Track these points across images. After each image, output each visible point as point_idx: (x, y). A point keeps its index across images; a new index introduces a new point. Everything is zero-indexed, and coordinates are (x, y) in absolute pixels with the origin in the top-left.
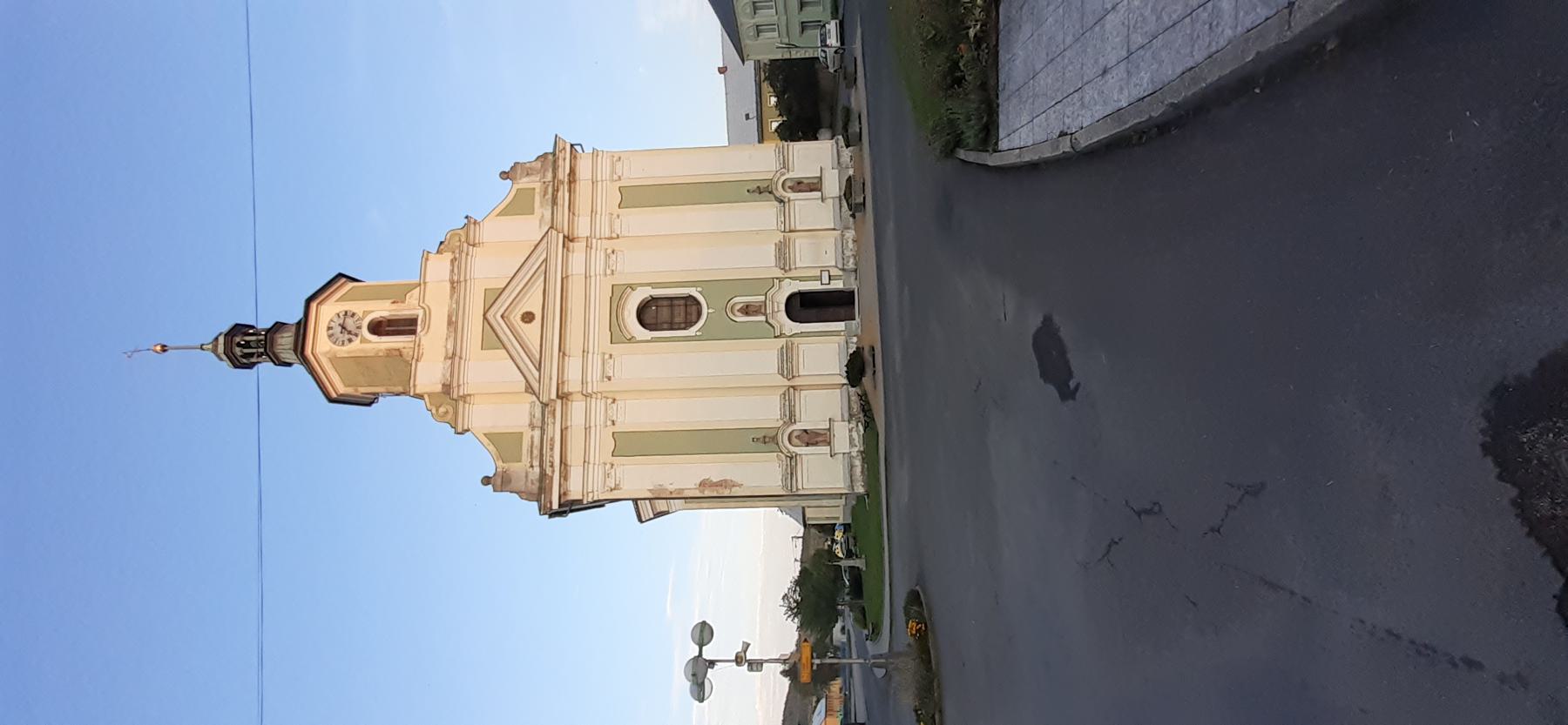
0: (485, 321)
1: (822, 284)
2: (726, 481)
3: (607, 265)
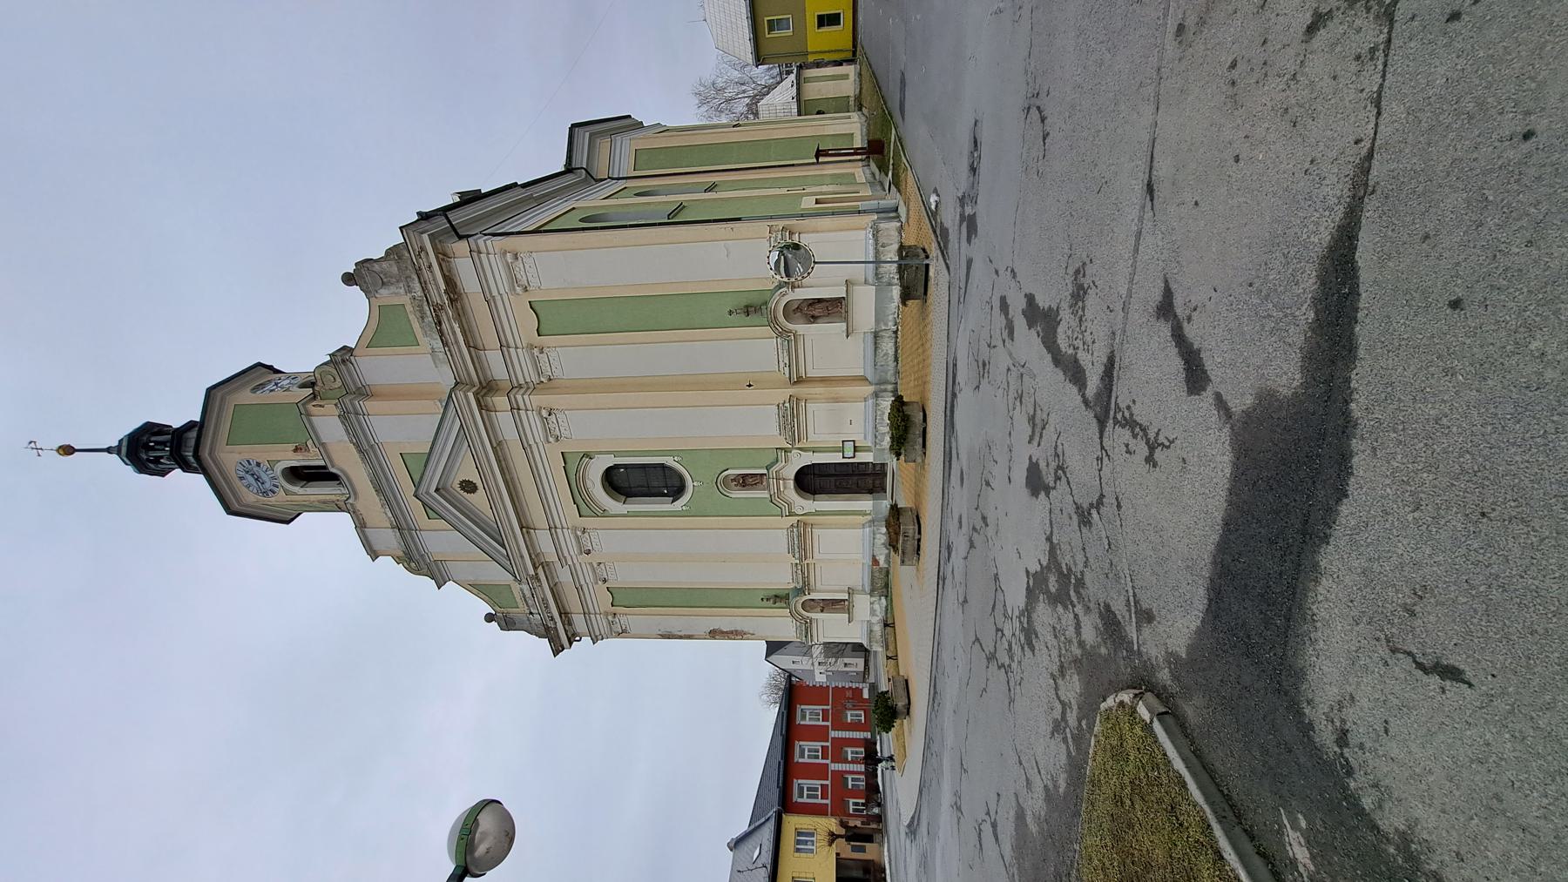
0: (417, 479)
1: (843, 457)
2: (736, 631)
3: (547, 431)
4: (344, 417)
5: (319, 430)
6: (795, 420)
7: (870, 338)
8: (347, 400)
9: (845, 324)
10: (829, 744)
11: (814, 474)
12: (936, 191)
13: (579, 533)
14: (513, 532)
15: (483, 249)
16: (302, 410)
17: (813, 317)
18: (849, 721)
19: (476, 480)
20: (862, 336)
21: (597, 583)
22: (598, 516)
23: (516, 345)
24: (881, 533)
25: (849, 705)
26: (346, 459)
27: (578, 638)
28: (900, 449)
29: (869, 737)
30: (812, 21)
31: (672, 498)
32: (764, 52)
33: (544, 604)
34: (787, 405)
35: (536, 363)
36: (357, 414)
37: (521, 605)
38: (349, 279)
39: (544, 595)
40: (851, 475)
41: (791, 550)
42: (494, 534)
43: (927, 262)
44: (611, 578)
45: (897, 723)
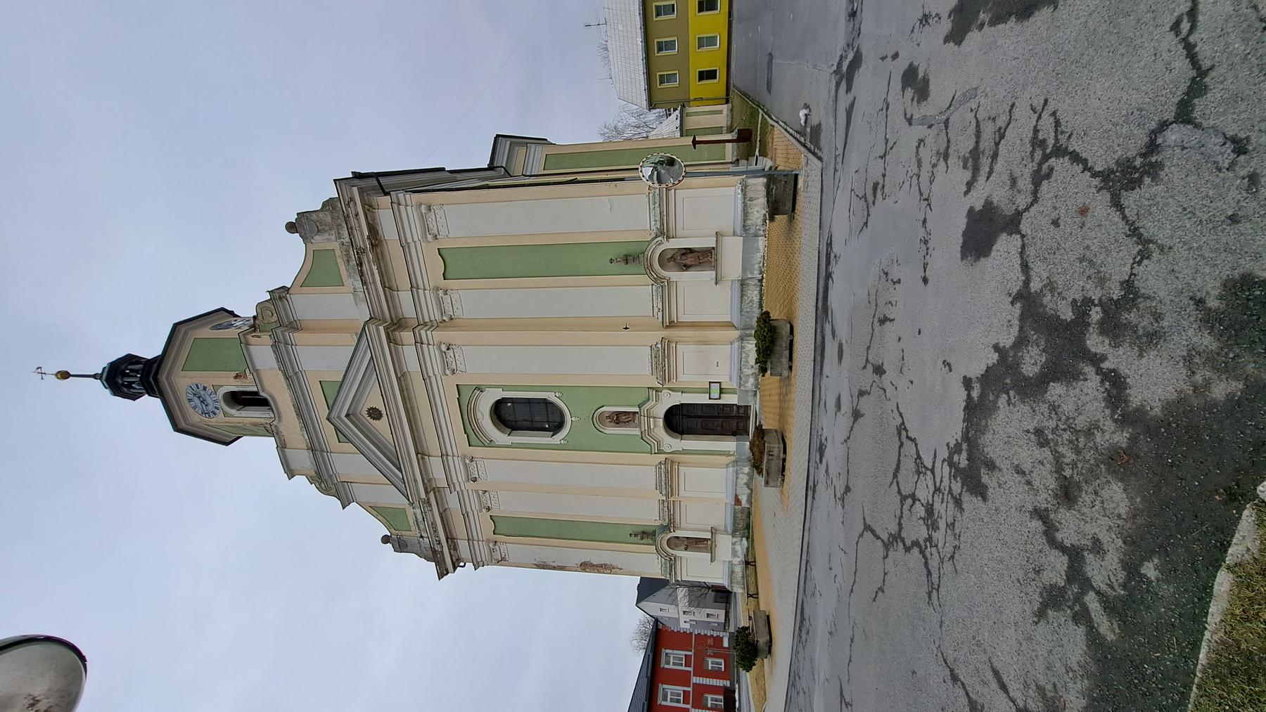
0: (330, 404)
1: (710, 399)
2: (605, 565)
3: (445, 365)
4: (275, 346)
5: (254, 357)
6: (666, 360)
7: (737, 286)
8: (279, 331)
9: (714, 273)
10: (690, 689)
11: (682, 415)
12: (807, 106)
13: (467, 461)
14: (410, 457)
15: (402, 201)
16: (243, 341)
17: (685, 266)
18: (710, 668)
19: (382, 408)
20: (730, 284)
21: (481, 511)
22: (485, 446)
23: (424, 287)
24: (743, 473)
25: (710, 652)
26: (275, 387)
27: (462, 564)
28: (766, 362)
29: (729, 685)
30: (694, 76)
31: (552, 433)
32: (655, 99)
33: (433, 528)
34: (659, 346)
35: (440, 303)
36: (286, 343)
37: (413, 528)
38: (291, 227)
39: (434, 520)
40: (716, 417)
41: (658, 486)
42: (394, 459)
43: (748, 607)
44: (494, 507)
45: (758, 661)
